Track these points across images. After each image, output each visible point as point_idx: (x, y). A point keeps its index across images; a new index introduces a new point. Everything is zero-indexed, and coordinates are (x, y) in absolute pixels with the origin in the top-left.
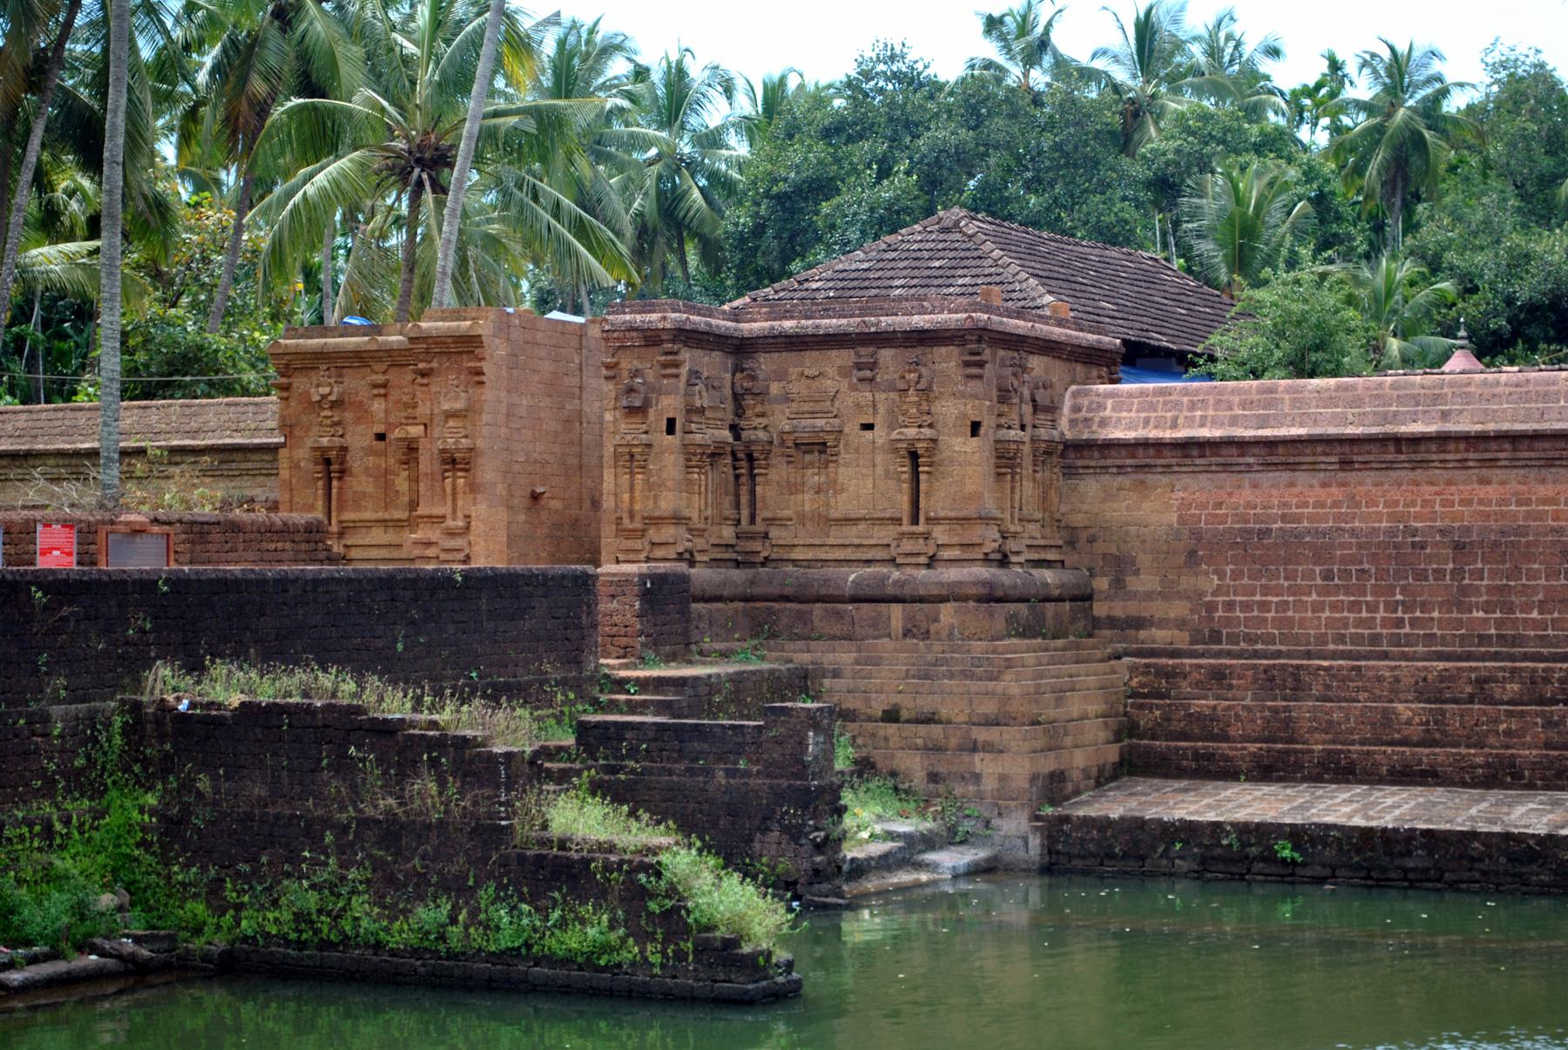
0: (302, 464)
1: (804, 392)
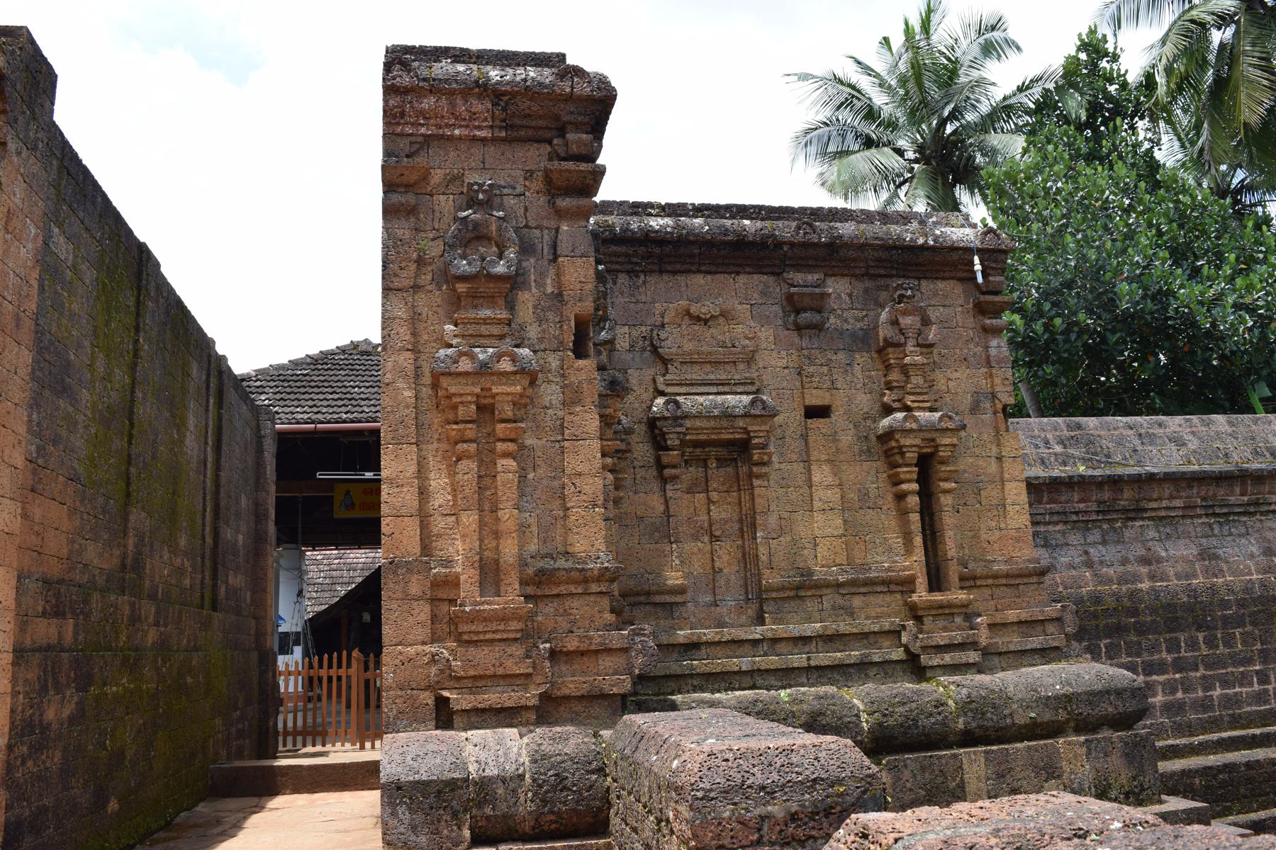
1: (689, 346)
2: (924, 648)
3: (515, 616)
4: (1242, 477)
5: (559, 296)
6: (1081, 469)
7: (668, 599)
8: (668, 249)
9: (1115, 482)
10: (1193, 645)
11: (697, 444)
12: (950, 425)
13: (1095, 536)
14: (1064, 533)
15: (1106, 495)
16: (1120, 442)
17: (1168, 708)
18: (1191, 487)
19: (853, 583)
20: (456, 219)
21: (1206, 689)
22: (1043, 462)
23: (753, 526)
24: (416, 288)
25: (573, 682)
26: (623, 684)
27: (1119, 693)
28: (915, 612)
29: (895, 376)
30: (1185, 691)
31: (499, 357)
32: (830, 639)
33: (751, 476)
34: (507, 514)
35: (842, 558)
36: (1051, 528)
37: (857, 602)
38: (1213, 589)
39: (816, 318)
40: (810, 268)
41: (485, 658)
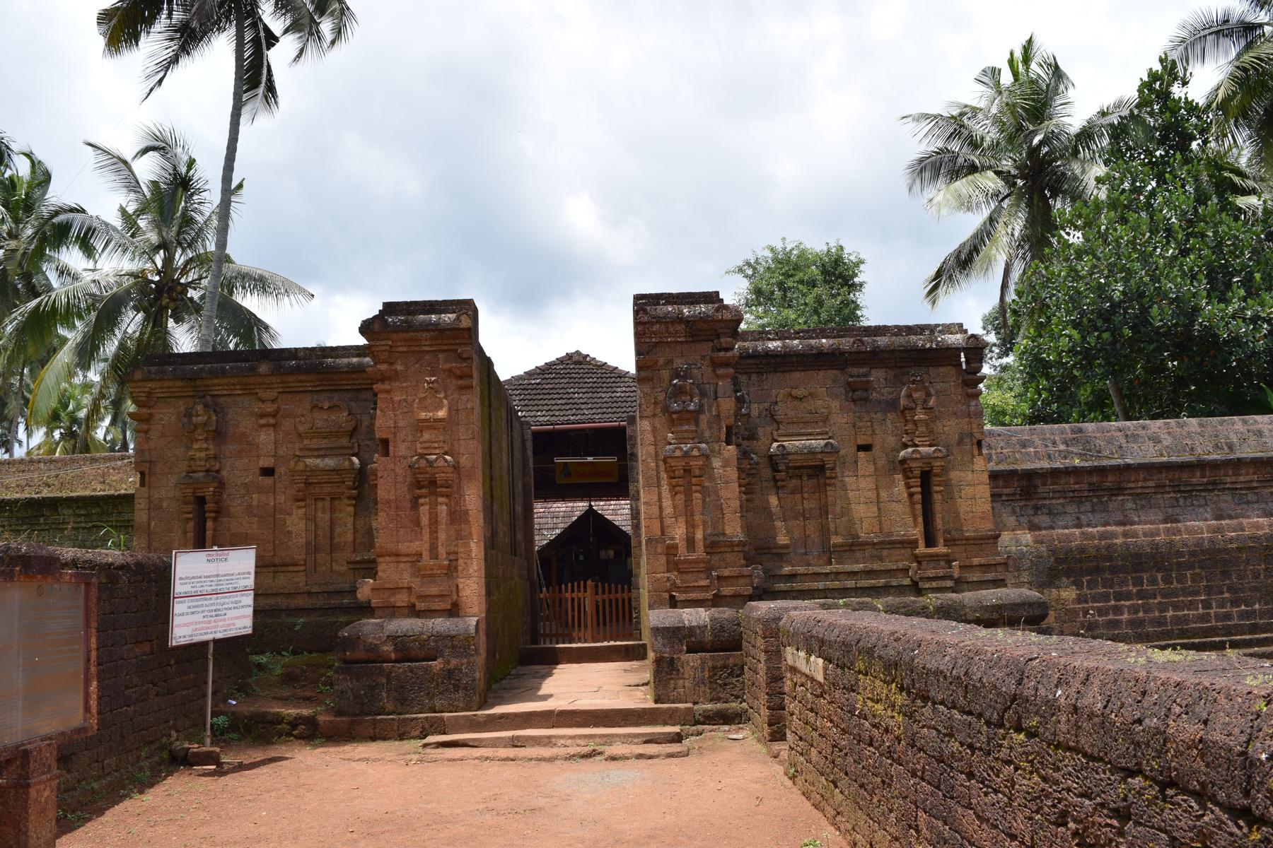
0: (165, 505)
1: (791, 413)
2: (921, 578)
3: (702, 561)
4: (1201, 465)
5: (718, 416)
6: (1077, 462)
7: (780, 551)
8: (779, 360)
9: (1101, 471)
10: (1153, 581)
11: (796, 468)
12: (940, 455)
13: (1087, 506)
14: (1063, 505)
15: (1095, 479)
16: (1110, 442)
17: (1131, 623)
18: (1161, 473)
19: (881, 543)
20: (671, 385)
21: (1161, 611)
22: (1049, 457)
23: (827, 513)
24: (654, 415)
25: (727, 591)
26: (750, 591)
27: (1031, 605)
28: (918, 559)
29: (910, 426)
30: (1145, 612)
31: (692, 449)
32: (869, 573)
33: (826, 485)
34: (697, 517)
35: (877, 529)
36: (1054, 501)
37: (885, 553)
38: (1171, 544)
39: (865, 394)
40: (861, 365)
41: (691, 580)
